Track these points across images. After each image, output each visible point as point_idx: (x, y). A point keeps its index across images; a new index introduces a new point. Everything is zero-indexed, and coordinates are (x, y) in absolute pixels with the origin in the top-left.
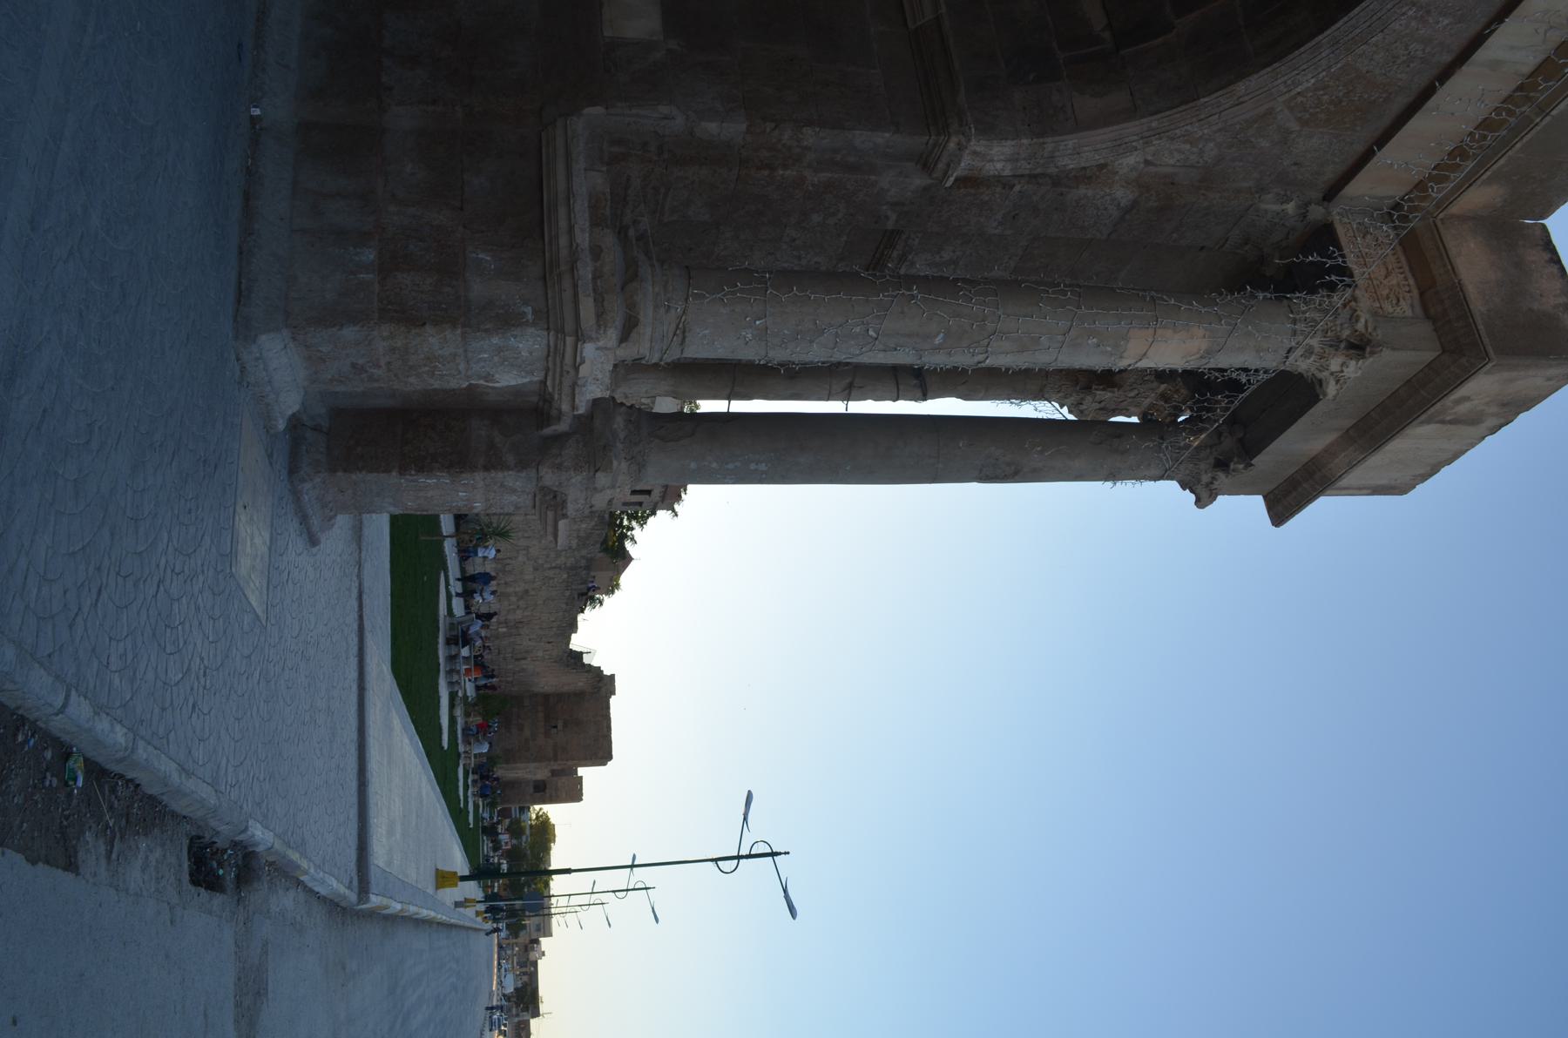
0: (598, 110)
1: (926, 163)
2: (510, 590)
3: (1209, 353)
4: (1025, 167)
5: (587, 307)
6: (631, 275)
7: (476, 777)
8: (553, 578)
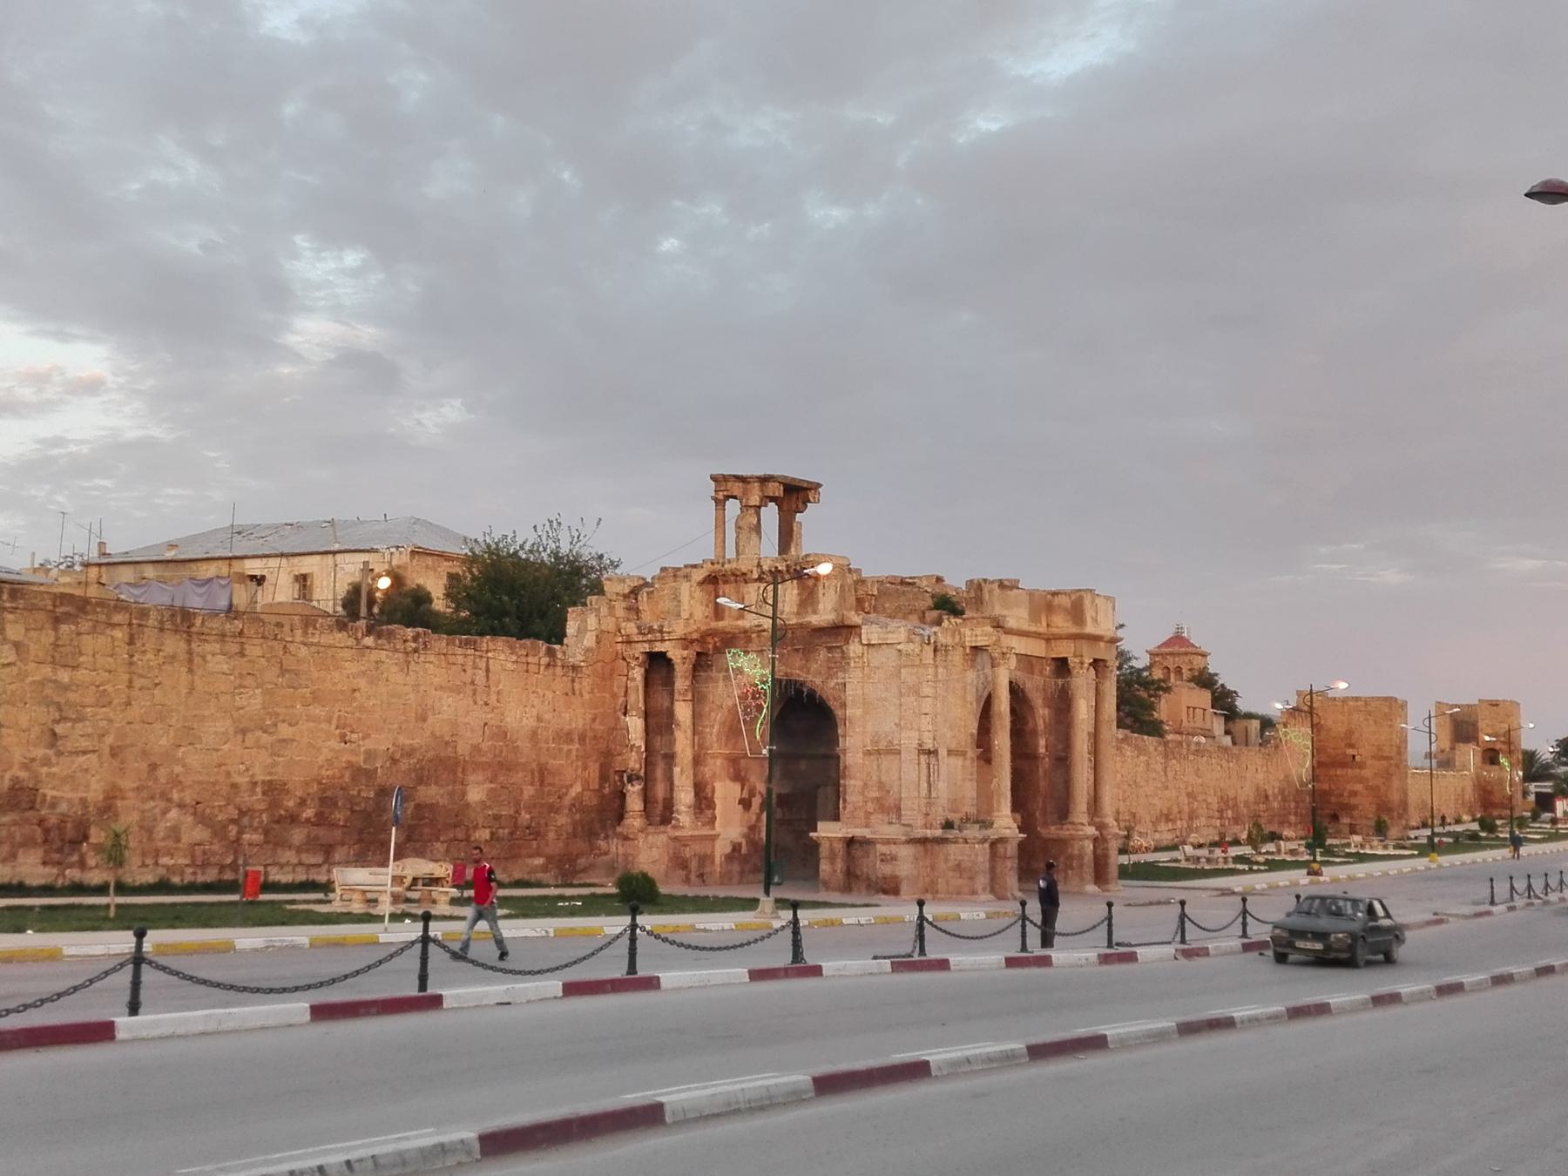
1: (1043, 758)
2: (1186, 808)
5: (1080, 833)
6: (1073, 823)
7: (1367, 846)
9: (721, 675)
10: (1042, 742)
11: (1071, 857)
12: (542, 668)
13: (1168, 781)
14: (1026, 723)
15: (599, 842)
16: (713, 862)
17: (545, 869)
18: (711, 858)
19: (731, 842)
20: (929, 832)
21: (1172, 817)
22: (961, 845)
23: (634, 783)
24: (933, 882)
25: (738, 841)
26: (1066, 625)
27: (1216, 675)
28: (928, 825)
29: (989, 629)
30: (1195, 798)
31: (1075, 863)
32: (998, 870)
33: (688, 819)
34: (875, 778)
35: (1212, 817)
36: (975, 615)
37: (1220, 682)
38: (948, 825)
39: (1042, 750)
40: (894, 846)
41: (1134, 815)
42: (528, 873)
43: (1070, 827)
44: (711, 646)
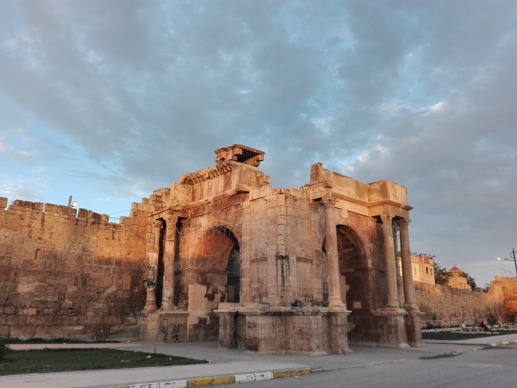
0: (371, 310)
1: (371, 271)
3: (391, 236)
4: (370, 258)
5: (394, 312)
6: (390, 306)
8: (456, 299)
9: (193, 229)
10: (370, 262)
11: (390, 327)
12: (89, 224)
13: (454, 302)
14: (360, 251)
15: (129, 318)
16: (186, 329)
17: (84, 332)
18: (185, 327)
19: (198, 318)
20: (283, 308)
21: (457, 315)
22: (301, 317)
23: (150, 286)
24: (286, 341)
25: (204, 317)
26: (378, 198)
27: (467, 274)
28: (283, 304)
29: (322, 188)
30: (465, 309)
31: (393, 330)
32: (333, 334)
33: (167, 305)
34: (256, 276)
35: (471, 316)
36: (315, 183)
37: (469, 276)
38: (295, 304)
39: (370, 265)
40: (255, 317)
41: (442, 314)
42: (69, 335)
43: (388, 308)
44: (190, 215)
